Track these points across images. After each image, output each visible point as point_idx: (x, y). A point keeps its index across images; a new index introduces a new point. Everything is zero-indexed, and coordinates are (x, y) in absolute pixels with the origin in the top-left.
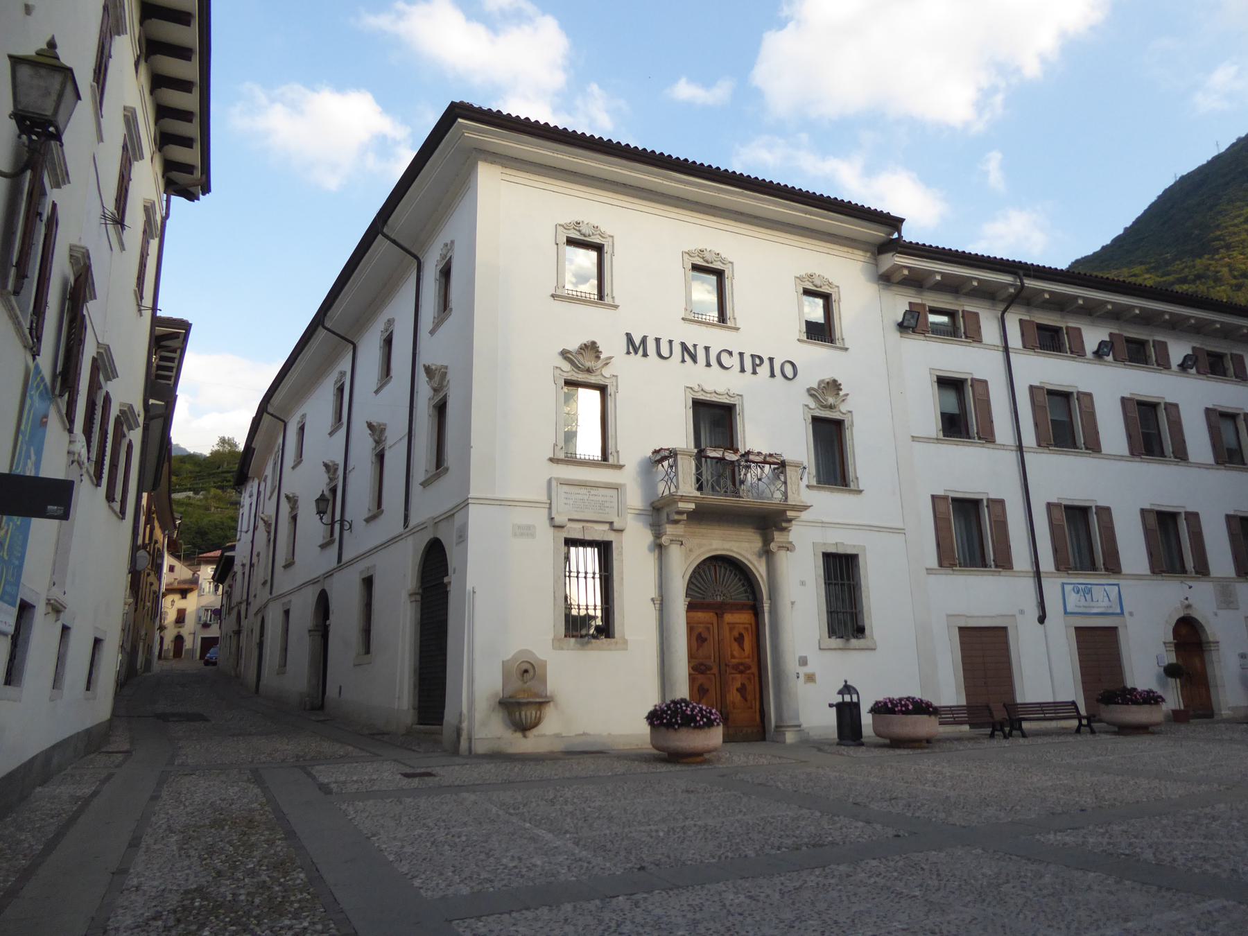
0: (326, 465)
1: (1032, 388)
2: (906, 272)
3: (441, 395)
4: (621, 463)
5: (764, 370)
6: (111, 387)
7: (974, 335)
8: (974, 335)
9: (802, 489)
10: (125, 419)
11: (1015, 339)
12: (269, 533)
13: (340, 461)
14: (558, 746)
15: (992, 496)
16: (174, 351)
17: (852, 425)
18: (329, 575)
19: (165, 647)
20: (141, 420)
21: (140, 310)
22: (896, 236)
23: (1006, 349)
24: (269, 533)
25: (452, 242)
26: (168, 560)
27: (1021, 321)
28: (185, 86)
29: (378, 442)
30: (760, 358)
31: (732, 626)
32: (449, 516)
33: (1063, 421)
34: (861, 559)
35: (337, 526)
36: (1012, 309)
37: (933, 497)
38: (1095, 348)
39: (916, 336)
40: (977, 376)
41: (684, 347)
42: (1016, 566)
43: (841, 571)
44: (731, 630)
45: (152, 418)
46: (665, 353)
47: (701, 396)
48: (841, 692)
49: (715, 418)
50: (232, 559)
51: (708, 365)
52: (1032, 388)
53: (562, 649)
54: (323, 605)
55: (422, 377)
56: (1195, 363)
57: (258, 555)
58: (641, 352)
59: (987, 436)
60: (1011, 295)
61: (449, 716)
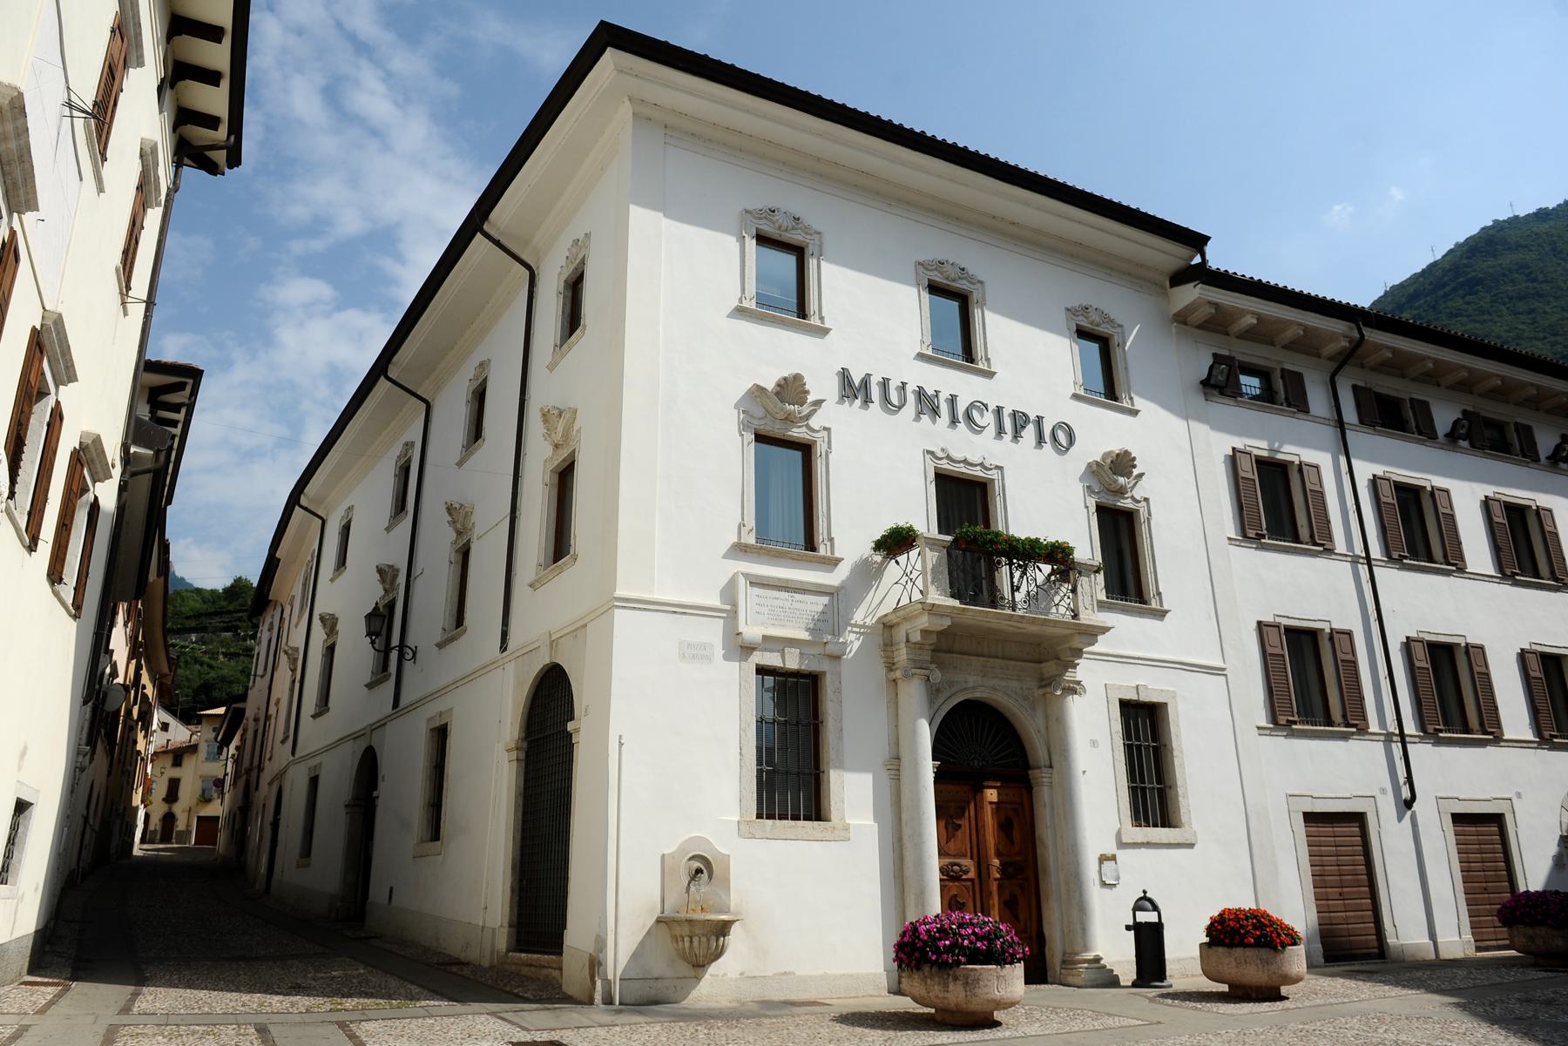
0: (380, 571)
3: (564, 453)
4: (837, 555)
5: (1029, 432)
6: (67, 395)
10: (87, 458)
12: (294, 671)
14: (753, 993)
16: (176, 408)
18: (380, 725)
19: (152, 827)
20: (117, 472)
21: (124, 303)
22: (1197, 260)
24: (294, 671)
25: (587, 235)
26: (159, 716)
28: (212, 78)
29: (459, 533)
32: (578, 630)
33: (1416, 530)
35: (394, 655)
36: (1347, 369)
38: (1448, 429)
39: (1226, 400)
41: (920, 393)
43: (1144, 725)
45: (134, 475)
46: (894, 398)
47: (945, 465)
48: (1137, 907)
49: (963, 497)
50: (243, 710)
54: (368, 769)
57: (278, 701)
61: (576, 936)
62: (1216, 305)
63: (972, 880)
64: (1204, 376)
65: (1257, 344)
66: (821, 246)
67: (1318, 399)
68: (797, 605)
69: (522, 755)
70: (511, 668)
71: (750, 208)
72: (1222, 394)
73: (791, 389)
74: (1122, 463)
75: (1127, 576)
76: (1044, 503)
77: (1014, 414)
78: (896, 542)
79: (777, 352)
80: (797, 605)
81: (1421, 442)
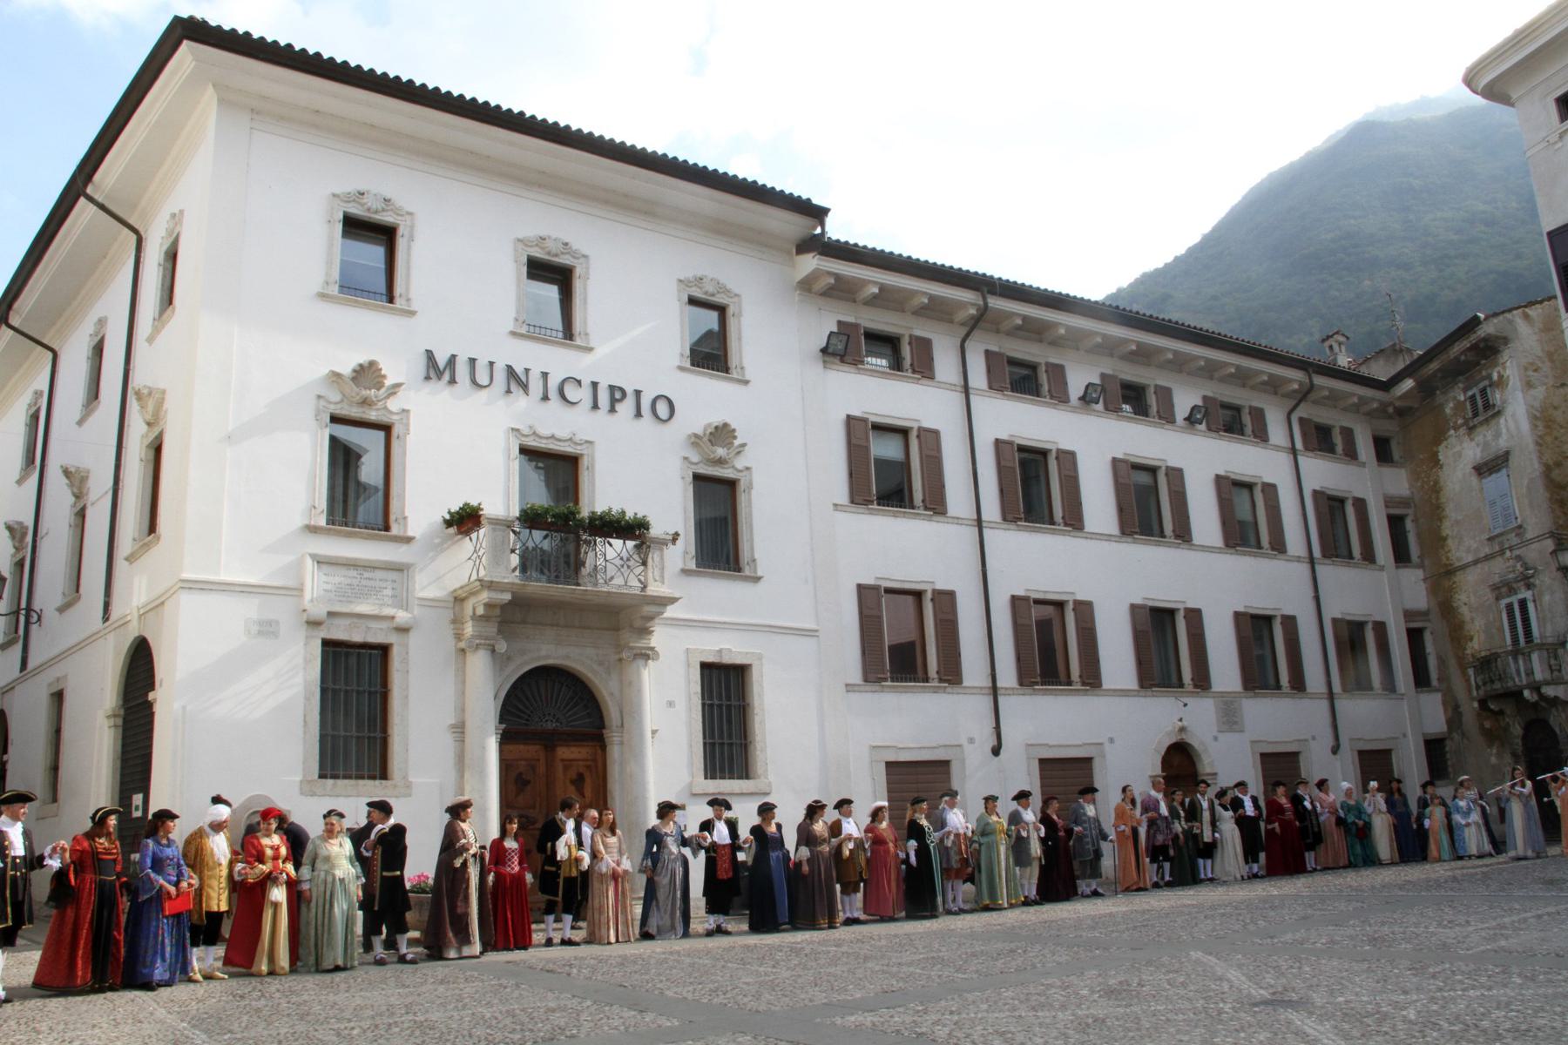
0: (9, 528)
1: (998, 442)
2: (1099, 340)
7: (1261, 435)
8: (924, 368)
9: (671, 571)
11: (978, 377)
13: (30, 523)
15: (939, 586)
17: (750, 487)
22: (818, 231)
23: (966, 390)
25: (181, 212)
27: (987, 352)
29: (78, 497)
30: (621, 389)
31: (568, 764)
33: (1034, 487)
34: (755, 674)
36: (976, 334)
37: (860, 587)
38: (1081, 393)
39: (846, 368)
40: (926, 424)
41: (510, 371)
42: (968, 680)
43: (725, 692)
44: (566, 768)
46: (482, 378)
49: (557, 467)
51: (545, 398)
52: (998, 442)
53: (313, 794)
55: (133, 404)
56: (1206, 415)
58: (447, 377)
59: (936, 505)
60: (972, 317)
62: (838, 277)
63: (1477, 823)
64: (824, 344)
65: (886, 309)
66: (412, 227)
67: (945, 363)
68: (364, 582)
69: (120, 721)
70: (111, 637)
71: (337, 191)
72: (842, 361)
73: (367, 373)
74: (722, 434)
75: (720, 540)
76: (636, 475)
77: (612, 388)
78: (466, 520)
79: (363, 336)
80: (364, 582)
81: (1054, 406)
